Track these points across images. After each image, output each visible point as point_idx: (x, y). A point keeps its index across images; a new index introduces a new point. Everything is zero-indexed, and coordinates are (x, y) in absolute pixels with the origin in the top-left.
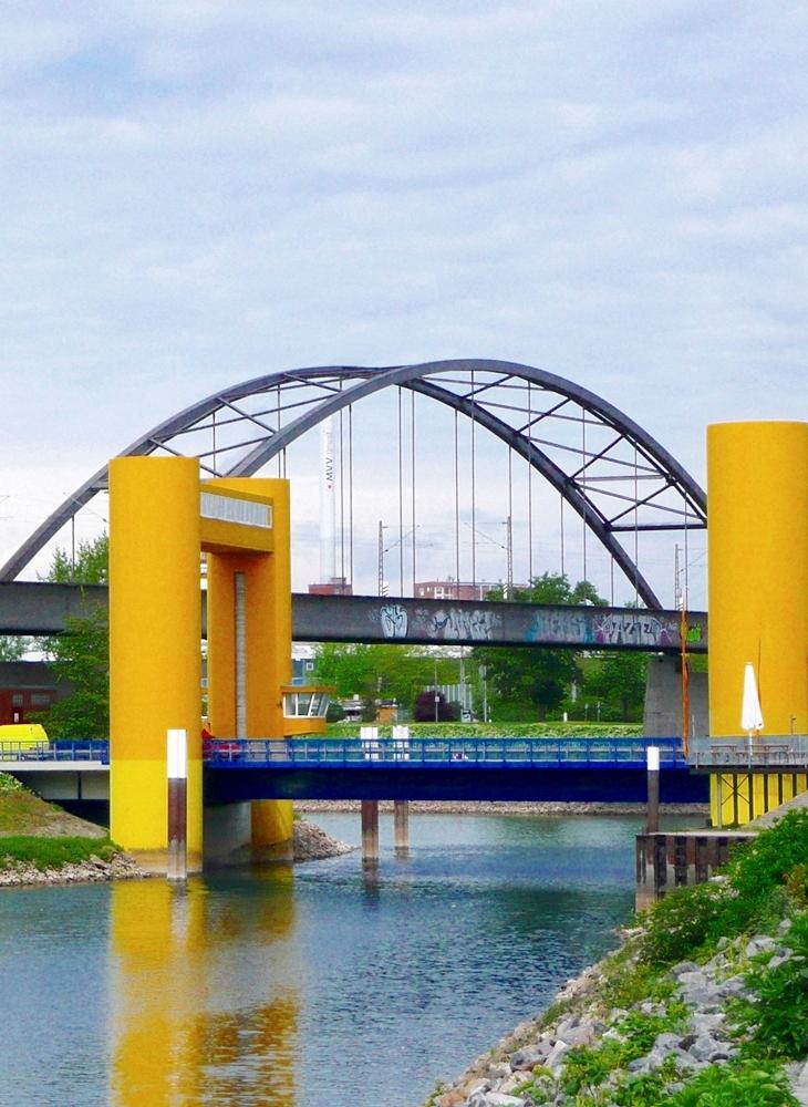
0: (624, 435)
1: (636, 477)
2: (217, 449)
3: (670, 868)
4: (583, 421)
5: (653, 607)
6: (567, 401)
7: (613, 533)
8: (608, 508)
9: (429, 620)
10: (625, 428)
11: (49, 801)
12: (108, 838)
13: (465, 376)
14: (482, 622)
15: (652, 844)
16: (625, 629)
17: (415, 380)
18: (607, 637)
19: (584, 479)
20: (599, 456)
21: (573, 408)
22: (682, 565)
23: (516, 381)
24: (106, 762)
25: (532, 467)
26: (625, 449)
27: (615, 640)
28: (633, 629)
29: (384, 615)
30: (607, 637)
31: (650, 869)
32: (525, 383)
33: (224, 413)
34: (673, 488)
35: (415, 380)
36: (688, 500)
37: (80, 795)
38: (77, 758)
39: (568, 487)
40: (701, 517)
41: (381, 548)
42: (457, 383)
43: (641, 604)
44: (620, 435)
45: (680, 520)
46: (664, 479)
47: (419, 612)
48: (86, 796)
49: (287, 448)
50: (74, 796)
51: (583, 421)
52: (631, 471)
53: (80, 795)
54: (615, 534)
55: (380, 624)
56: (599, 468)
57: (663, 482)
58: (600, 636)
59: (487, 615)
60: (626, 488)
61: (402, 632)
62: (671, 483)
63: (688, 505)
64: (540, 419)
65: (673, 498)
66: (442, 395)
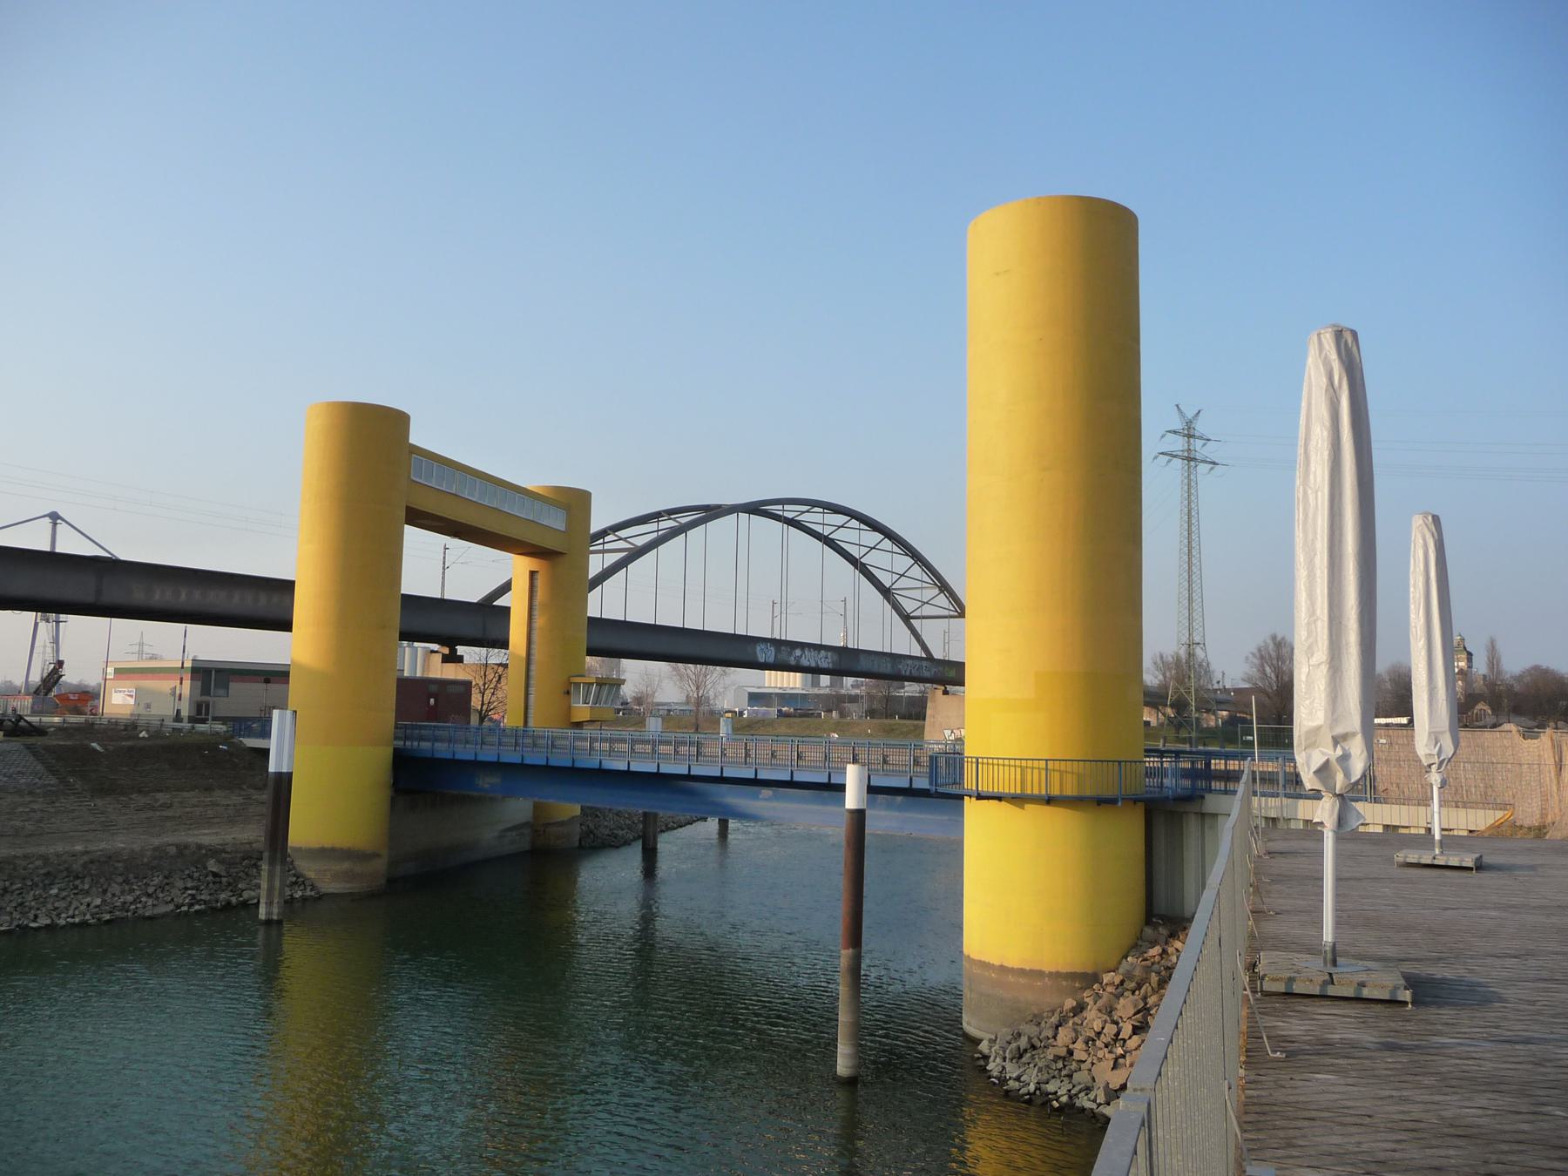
0: (916, 562)
1: (922, 588)
4: (860, 529)
5: (930, 658)
8: (908, 606)
9: (790, 654)
10: (917, 557)
13: (780, 507)
14: (827, 658)
17: (755, 509)
18: (903, 672)
19: (894, 589)
20: (872, 548)
21: (854, 523)
22: (947, 641)
23: (816, 509)
26: (917, 571)
27: (908, 673)
29: (758, 648)
30: (903, 672)
32: (821, 510)
35: (755, 509)
36: (923, 570)
39: (886, 592)
40: (957, 611)
41: (444, 563)
42: (790, 512)
43: (924, 655)
45: (946, 613)
47: (783, 648)
51: (860, 529)
52: (919, 584)
55: (755, 653)
56: (903, 582)
57: (937, 591)
58: (900, 670)
59: (829, 654)
60: (916, 594)
61: (771, 660)
62: (941, 591)
63: (924, 573)
64: (845, 523)
65: (942, 600)
66: (160, 596)
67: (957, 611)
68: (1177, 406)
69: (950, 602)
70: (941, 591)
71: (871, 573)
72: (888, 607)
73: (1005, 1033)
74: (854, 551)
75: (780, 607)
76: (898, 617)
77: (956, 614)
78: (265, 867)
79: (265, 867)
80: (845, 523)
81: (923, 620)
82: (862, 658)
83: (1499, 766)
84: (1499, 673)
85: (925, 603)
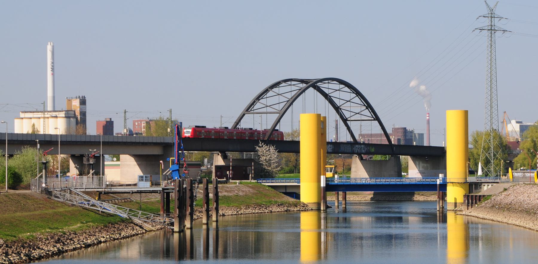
0: (357, 96)
2: (278, 104)
3: (470, 201)
6: (345, 87)
7: (347, 122)
10: (358, 93)
11: (281, 192)
12: (300, 201)
15: (467, 197)
16: (359, 149)
21: (347, 89)
24: (299, 182)
25: (329, 103)
26: (357, 100)
28: (360, 149)
31: (467, 201)
33: (270, 93)
34: (367, 110)
37: (286, 191)
38: (272, 182)
39: (337, 109)
40: (373, 117)
41: (221, 122)
44: (356, 95)
46: (365, 107)
48: (287, 191)
49: (293, 104)
50: (284, 191)
53: (286, 191)
54: (347, 122)
57: (365, 108)
58: (354, 151)
62: (367, 108)
64: (346, 103)
65: (367, 112)
67: (373, 117)
68: (485, 1)
69: (361, 101)
70: (367, 108)
71: (322, 90)
72: (327, 102)
73: (350, 220)
74: (338, 102)
75: (471, 181)
76: (330, 105)
77: (373, 119)
78: (198, 223)
79: (198, 223)
80: (346, 103)
81: (362, 121)
82: (445, 170)
83: (242, 215)
84: (316, 203)
85: (349, 101)
